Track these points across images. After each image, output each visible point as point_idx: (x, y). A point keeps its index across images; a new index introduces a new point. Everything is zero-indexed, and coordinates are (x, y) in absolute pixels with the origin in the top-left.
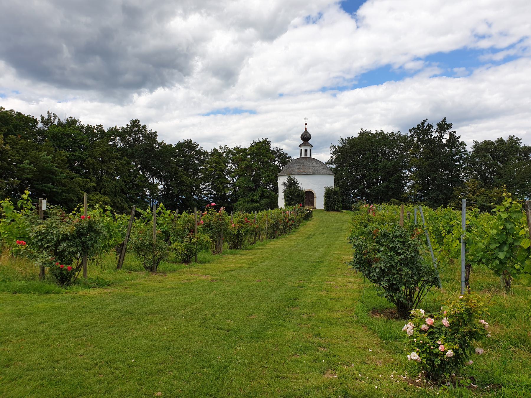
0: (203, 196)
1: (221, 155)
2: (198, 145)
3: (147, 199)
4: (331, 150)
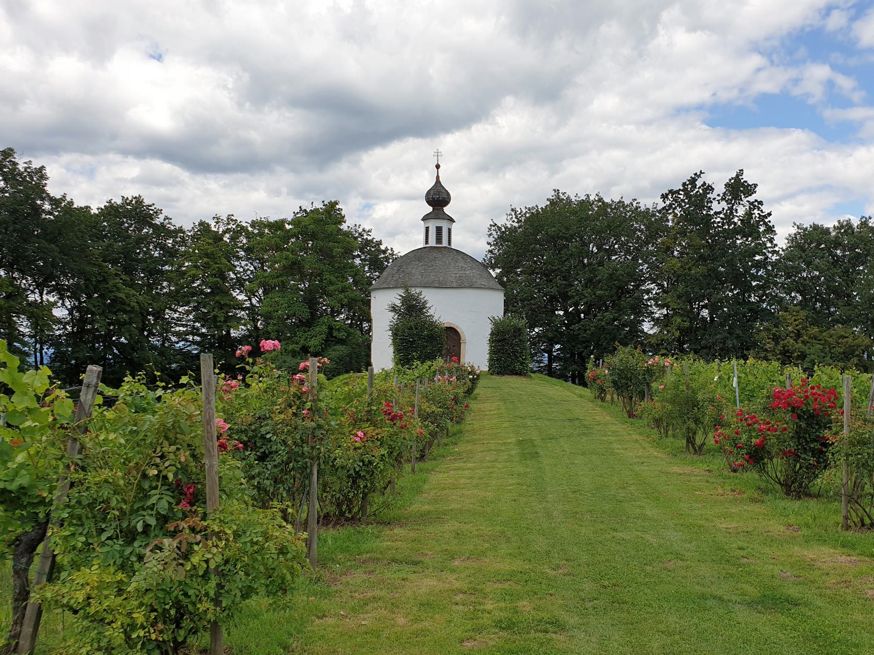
0: (174, 339)
1: (218, 238)
2: (158, 212)
3: (25, 344)
4: (491, 235)
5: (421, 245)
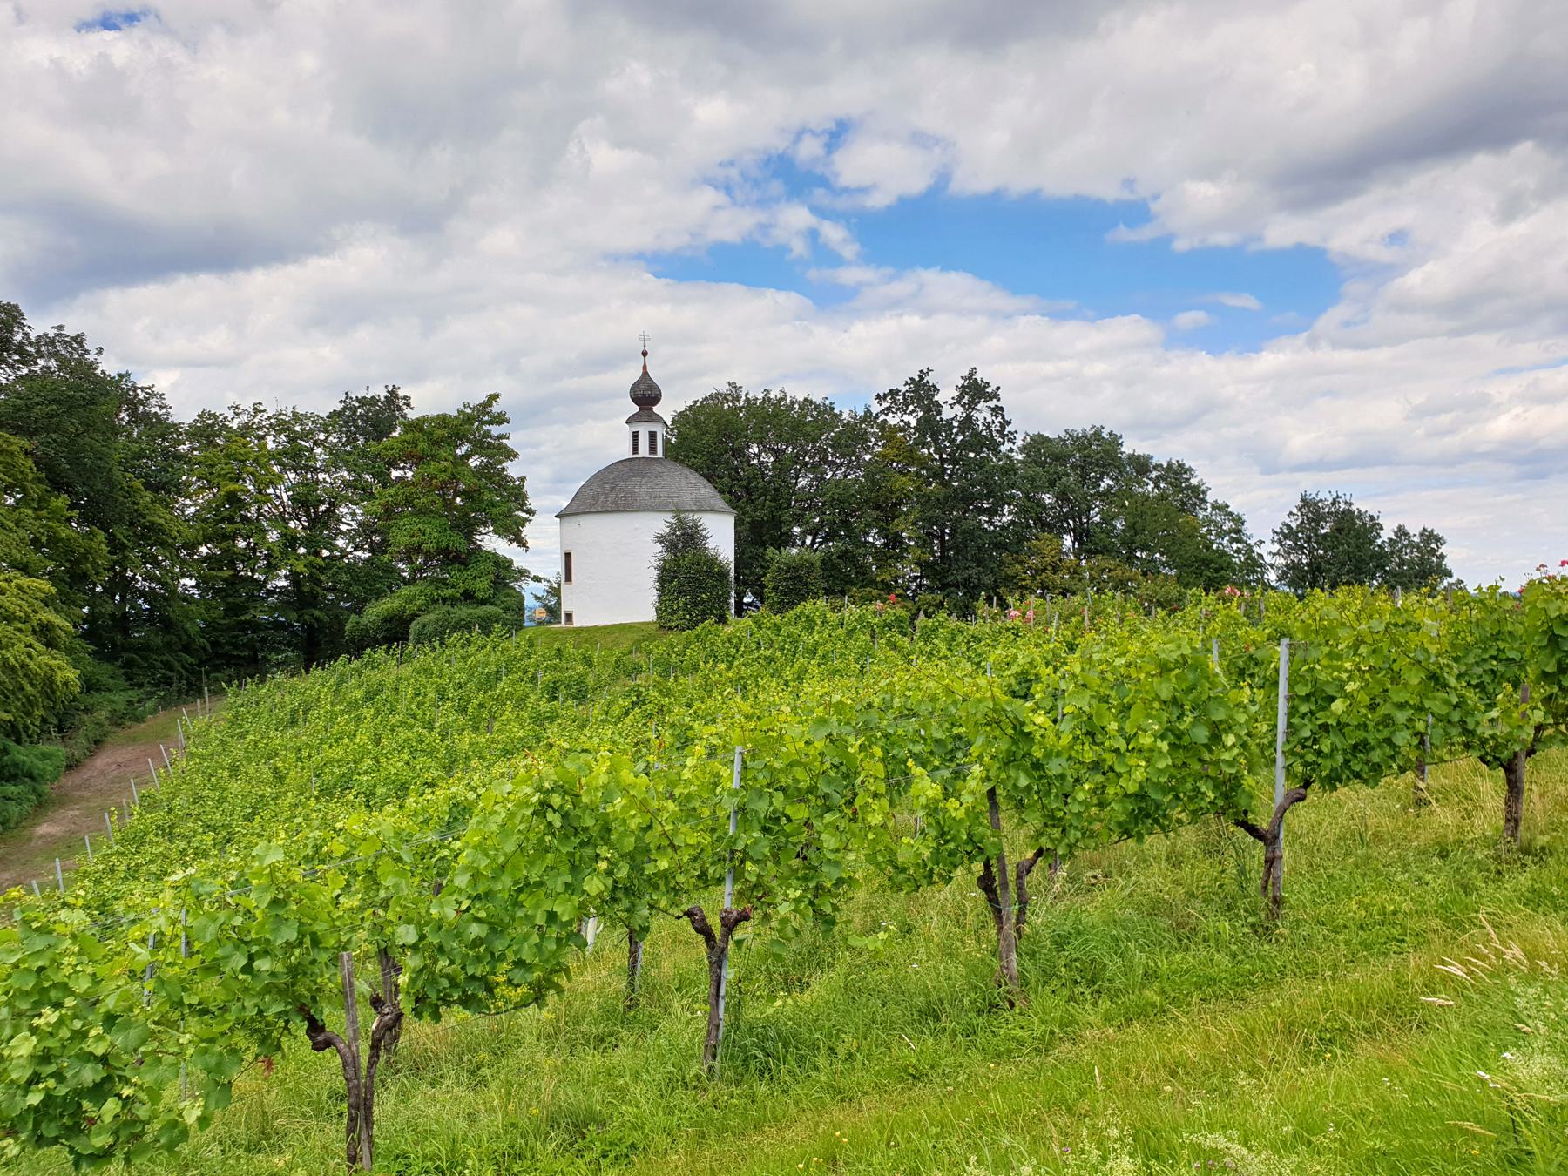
5: (627, 453)
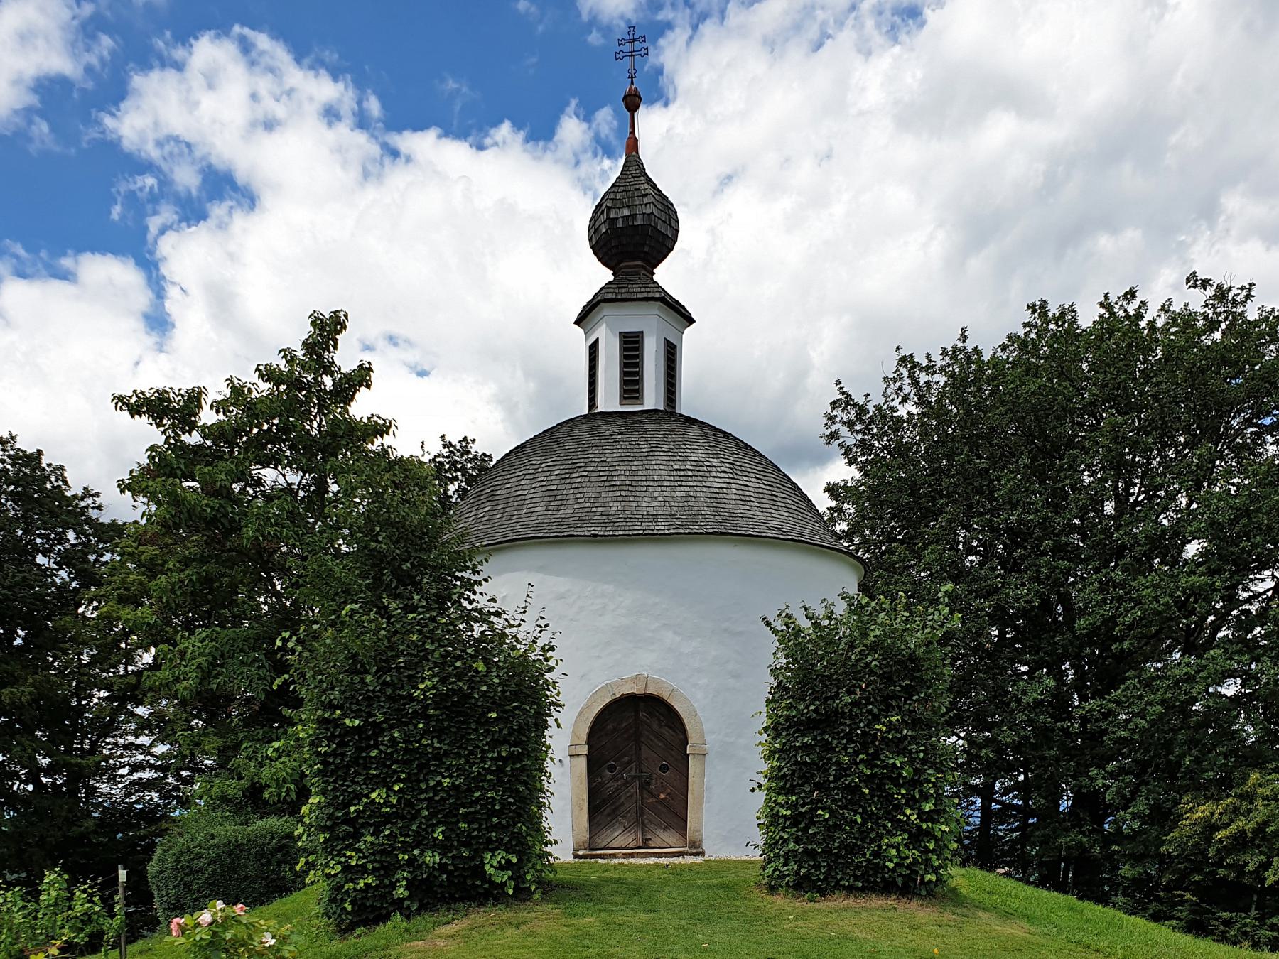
4: (834, 436)
